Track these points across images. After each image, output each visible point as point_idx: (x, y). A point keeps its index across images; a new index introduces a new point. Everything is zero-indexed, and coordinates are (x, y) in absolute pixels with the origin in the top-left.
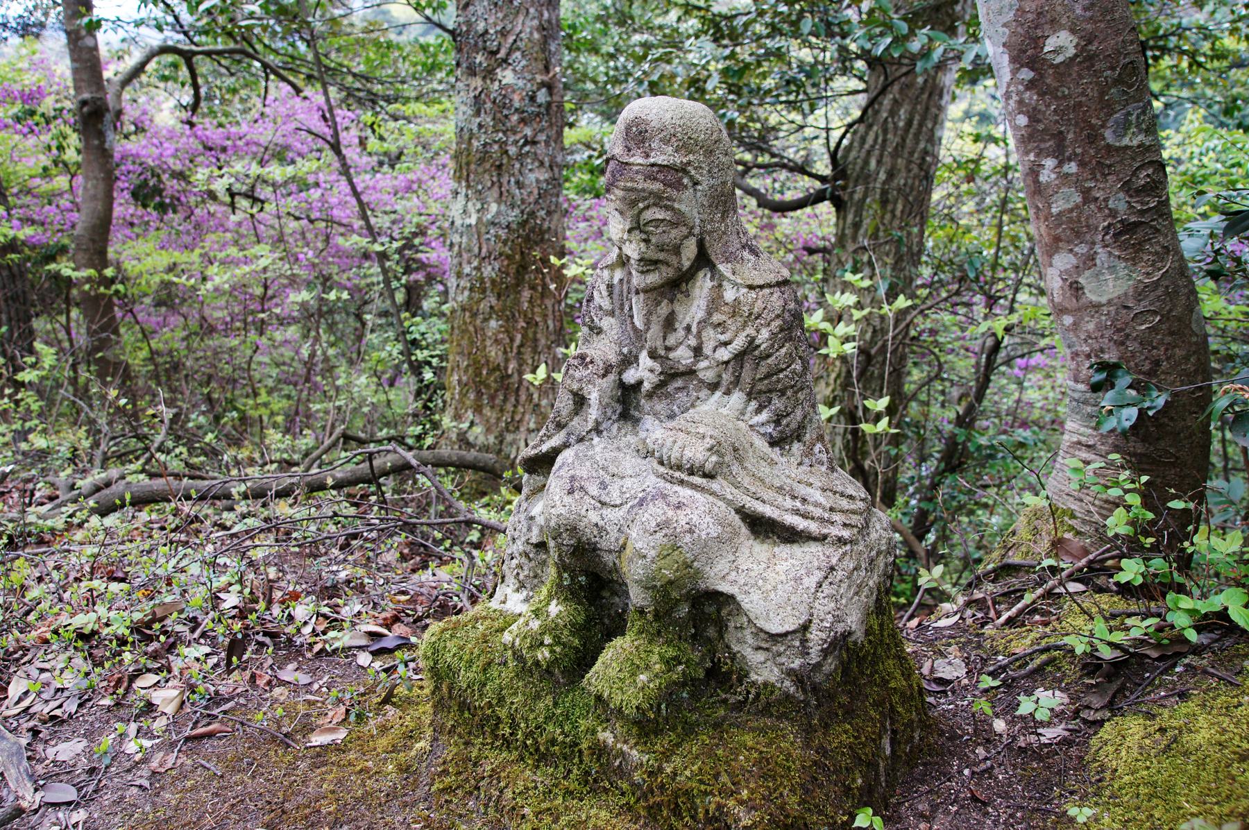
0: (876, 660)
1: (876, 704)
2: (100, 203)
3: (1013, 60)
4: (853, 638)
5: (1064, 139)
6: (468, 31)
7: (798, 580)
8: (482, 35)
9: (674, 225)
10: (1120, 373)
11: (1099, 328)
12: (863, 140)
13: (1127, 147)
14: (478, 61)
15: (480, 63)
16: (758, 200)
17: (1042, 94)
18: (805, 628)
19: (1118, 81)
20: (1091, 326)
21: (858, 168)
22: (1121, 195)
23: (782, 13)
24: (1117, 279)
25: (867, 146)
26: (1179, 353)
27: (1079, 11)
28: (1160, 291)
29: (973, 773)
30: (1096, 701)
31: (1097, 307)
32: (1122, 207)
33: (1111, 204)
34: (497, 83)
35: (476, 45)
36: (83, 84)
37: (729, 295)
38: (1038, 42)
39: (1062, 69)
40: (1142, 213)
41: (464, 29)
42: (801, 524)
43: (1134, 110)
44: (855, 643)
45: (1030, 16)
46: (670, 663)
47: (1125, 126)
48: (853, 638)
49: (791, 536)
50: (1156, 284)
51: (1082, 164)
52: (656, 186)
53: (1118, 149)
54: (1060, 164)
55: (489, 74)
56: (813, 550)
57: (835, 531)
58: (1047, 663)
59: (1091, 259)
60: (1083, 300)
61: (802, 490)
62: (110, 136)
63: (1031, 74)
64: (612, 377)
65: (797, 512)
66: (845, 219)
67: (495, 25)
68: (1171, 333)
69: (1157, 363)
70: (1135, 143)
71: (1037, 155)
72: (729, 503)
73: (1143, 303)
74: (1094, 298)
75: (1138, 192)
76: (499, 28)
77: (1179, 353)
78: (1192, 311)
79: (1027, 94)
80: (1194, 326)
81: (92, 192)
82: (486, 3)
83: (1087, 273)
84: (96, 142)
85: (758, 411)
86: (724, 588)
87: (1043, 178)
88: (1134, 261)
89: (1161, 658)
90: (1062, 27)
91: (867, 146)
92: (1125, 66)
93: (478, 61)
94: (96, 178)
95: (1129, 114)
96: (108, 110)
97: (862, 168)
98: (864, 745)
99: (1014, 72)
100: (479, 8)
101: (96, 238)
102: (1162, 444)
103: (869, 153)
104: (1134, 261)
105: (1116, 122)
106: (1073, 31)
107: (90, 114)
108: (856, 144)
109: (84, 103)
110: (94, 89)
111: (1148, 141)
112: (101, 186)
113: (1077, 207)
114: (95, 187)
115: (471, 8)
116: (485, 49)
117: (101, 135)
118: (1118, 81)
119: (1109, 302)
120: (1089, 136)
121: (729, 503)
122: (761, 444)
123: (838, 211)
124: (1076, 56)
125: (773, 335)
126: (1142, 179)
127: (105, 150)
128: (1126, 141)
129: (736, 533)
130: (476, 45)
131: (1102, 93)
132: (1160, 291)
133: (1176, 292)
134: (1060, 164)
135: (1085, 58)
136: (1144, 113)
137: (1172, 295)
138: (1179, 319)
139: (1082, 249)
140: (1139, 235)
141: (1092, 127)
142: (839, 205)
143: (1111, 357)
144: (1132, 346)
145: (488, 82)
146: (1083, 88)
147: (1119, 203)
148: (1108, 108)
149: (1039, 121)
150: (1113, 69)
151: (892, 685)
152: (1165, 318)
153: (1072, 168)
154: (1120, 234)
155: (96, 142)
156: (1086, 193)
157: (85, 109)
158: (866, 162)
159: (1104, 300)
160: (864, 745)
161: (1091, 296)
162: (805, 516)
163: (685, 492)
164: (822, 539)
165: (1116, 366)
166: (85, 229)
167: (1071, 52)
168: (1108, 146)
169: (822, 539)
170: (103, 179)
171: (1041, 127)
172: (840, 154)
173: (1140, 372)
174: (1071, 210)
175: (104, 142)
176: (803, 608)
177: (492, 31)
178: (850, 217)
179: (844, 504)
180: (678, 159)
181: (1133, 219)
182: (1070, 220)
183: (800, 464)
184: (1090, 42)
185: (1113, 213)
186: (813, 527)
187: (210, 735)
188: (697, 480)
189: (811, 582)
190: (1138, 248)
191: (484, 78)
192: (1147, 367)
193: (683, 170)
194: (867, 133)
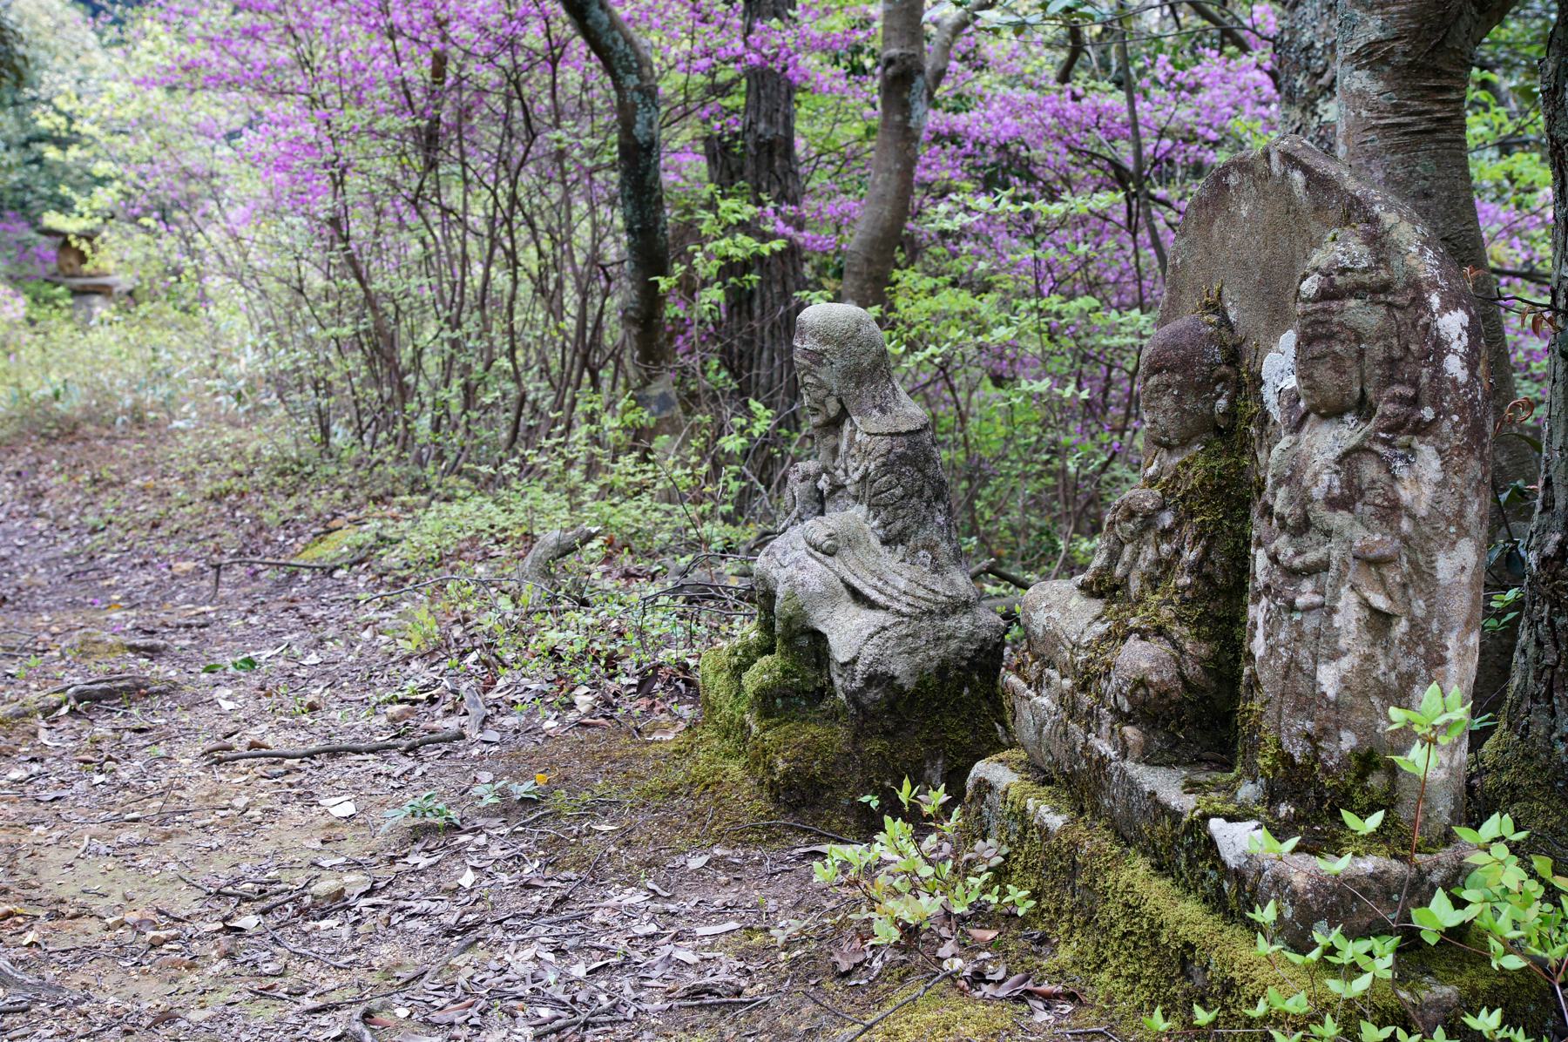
2: (888, 207)
6: (1290, 41)
7: (860, 630)
8: (1307, 49)
9: (820, 387)
14: (1298, 84)
15: (1302, 88)
18: (854, 661)
34: (1316, 118)
35: (1297, 62)
36: (893, 34)
37: (858, 437)
41: (1287, 38)
42: (874, 595)
46: (785, 672)
49: (873, 605)
52: (807, 362)
55: (1309, 106)
56: (879, 617)
57: (896, 606)
61: (890, 577)
62: (919, 107)
64: (809, 483)
65: (875, 588)
67: (1326, 35)
72: (837, 574)
76: (1328, 41)
81: (880, 190)
82: (1317, 5)
84: (898, 118)
85: (875, 517)
86: (822, 628)
93: (1298, 84)
94: (889, 171)
96: (921, 71)
100: (1309, 10)
101: (875, 258)
107: (895, 78)
109: (890, 61)
110: (906, 41)
112: (895, 181)
114: (886, 183)
115: (1300, 8)
116: (1308, 69)
117: (906, 108)
121: (837, 574)
122: (875, 542)
125: (877, 468)
127: (909, 129)
129: (837, 594)
130: (1297, 62)
145: (1308, 115)
155: (898, 118)
157: (890, 71)
162: (881, 592)
163: (811, 561)
164: (887, 608)
166: (861, 243)
169: (887, 608)
170: (899, 172)
175: (910, 117)
176: (855, 648)
177: (1319, 45)
179: (931, 596)
180: (818, 347)
183: (903, 561)
186: (882, 599)
187: (594, 725)
188: (818, 554)
189: (866, 633)
191: (1304, 109)
193: (822, 353)
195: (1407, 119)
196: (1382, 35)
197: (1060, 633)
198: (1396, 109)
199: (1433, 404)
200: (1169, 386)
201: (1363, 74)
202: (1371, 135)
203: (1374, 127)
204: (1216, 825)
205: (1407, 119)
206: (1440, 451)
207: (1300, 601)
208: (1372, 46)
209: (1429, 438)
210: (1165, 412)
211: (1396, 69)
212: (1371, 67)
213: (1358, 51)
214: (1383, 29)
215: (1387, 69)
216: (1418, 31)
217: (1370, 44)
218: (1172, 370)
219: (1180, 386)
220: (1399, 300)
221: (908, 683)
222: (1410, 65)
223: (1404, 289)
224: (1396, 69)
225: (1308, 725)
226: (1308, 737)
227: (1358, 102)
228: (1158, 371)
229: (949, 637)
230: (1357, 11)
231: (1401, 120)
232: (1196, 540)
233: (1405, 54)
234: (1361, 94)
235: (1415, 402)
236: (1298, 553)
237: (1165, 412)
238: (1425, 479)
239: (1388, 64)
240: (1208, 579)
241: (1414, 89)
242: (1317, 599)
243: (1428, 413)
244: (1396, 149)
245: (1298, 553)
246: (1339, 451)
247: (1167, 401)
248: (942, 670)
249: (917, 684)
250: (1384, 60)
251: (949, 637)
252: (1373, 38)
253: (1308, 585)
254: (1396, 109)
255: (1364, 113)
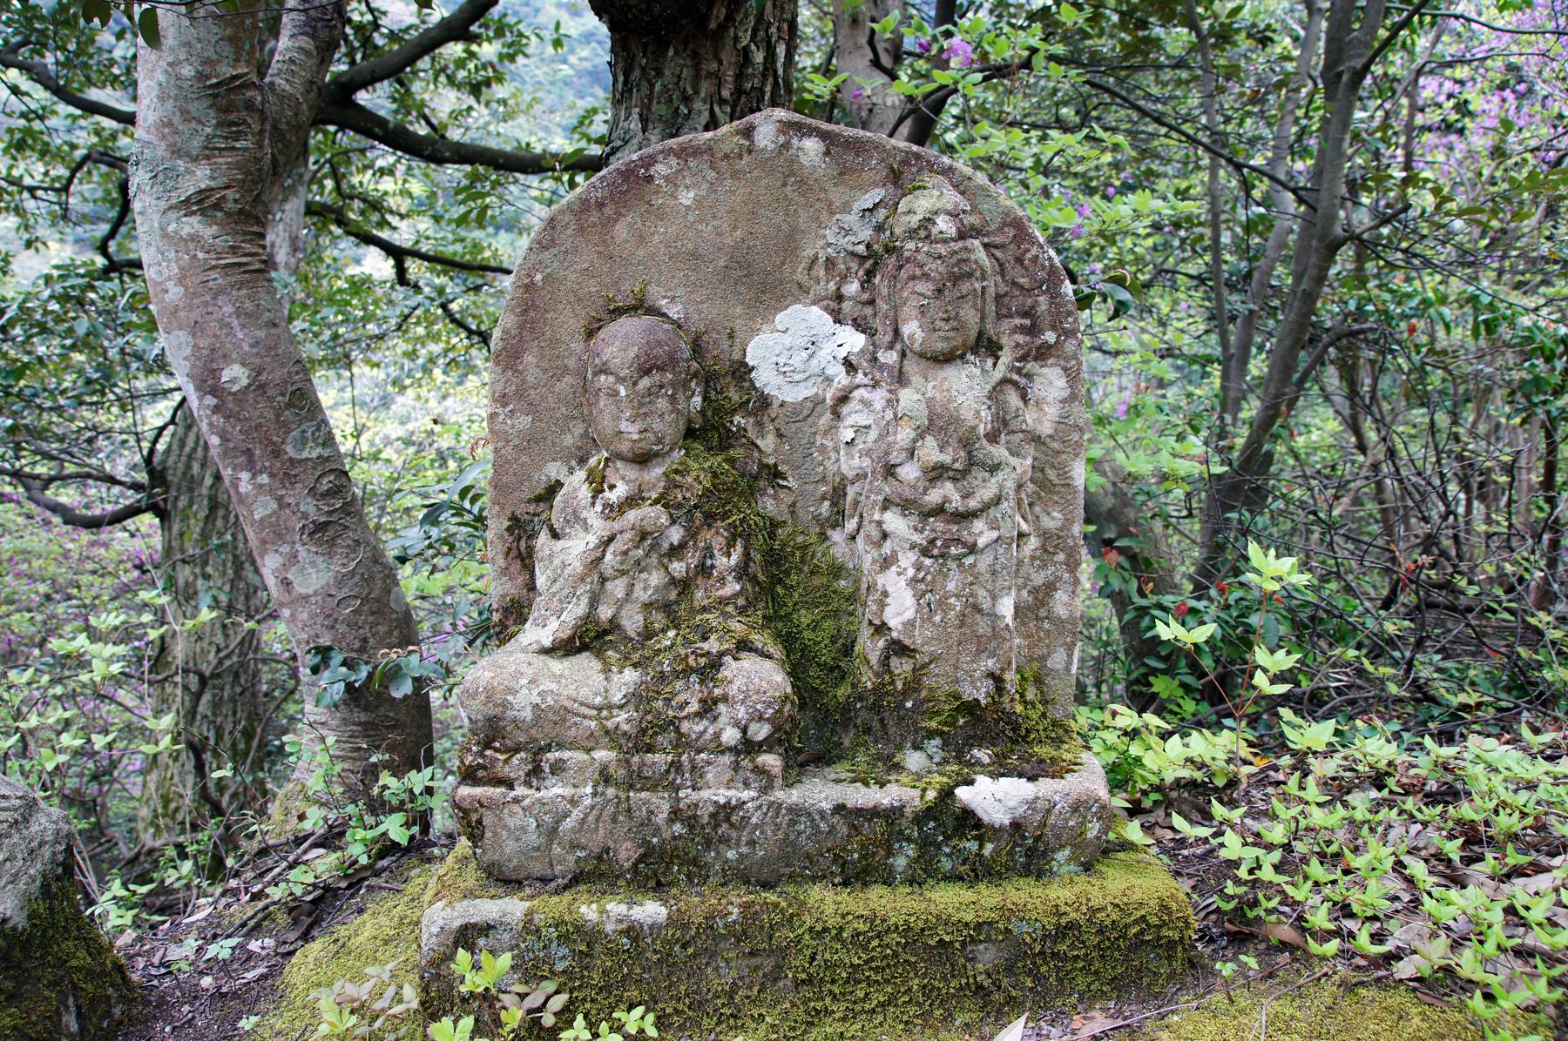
0: (46, 943)
1: (52, 985)
3: (198, 388)
4: (11, 924)
5: (253, 455)
10: (333, 654)
11: (312, 616)
12: (182, 443)
13: (307, 459)
16: (63, 516)
17: (227, 417)
19: (289, 405)
20: (305, 616)
21: (179, 473)
22: (309, 499)
23: (53, 312)
24: (318, 572)
25: (187, 450)
26: (382, 629)
27: (246, 348)
28: (357, 578)
29: (174, 1028)
30: (292, 936)
31: (306, 598)
32: (311, 510)
33: (302, 508)
38: (215, 373)
39: (240, 396)
40: (330, 513)
43: (310, 428)
44: (14, 928)
45: (205, 352)
47: (303, 441)
48: (11, 924)
50: (353, 573)
51: (272, 475)
53: (300, 461)
54: (254, 476)
58: (264, 919)
59: (293, 557)
60: (294, 594)
63: (214, 401)
66: (170, 529)
68: (373, 613)
69: (365, 640)
70: (314, 455)
71: (234, 469)
73: (345, 590)
74: (303, 591)
75: (324, 496)
77: (382, 629)
78: (389, 592)
79: (215, 418)
80: (392, 605)
83: (293, 569)
87: (242, 490)
88: (330, 555)
89: (349, 887)
90: (233, 361)
91: (187, 450)
92: (293, 393)
95: (304, 431)
97: (184, 474)
98: (35, 1024)
99: (201, 399)
102: (382, 711)
103: (190, 457)
104: (330, 555)
105: (295, 439)
106: (243, 364)
108: (175, 447)
111: (326, 453)
113: (274, 512)
118: (289, 405)
119: (316, 593)
120: (273, 452)
123: (162, 521)
124: (250, 385)
126: (325, 485)
128: (305, 454)
131: (278, 416)
132: (357, 578)
133: (372, 578)
134: (254, 476)
135: (258, 386)
136: (318, 429)
137: (368, 580)
138: (378, 600)
139: (285, 549)
140: (330, 532)
141: (274, 444)
142: (162, 514)
143: (325, 641)
144: (342, 628)
146: (260, 411)
147: (309, 506)
148: (286, 427)
149: (228, 440)
150: (283, 395)
151: (74, 963)
152: (365, 600)
153: (264, 479)
154: (314, 532)
156: (280, 499)
158: (188, 467)
159: (310, 591)
160: (35, 1024)
161: (300, 589)
165: (330, 649)
167: (245, 382)
168: (291, 459)
171: (231, 445)
172: (156, 459)
173: (353, 650)
174: (270, 516)
178: (176, 528)
181: (323, 519)
182: (271, 525)
184: (259, 373)
185: (305, 516)
190: (332, 543)
192: (357, 645)
194: (186, 435)
195: (244, 260)
196: (213, 184)
197: (569, 704)
198: (234, 250)
199: (1053, 328)
200: (661, 387)
201: (195, 220)
202: (213, 275)
203: (214, 267)
204: (962, 793)
205: (244, 260)
206: (1065, 369)
207: (981, 542)
208: (204, 195)
209: (1051, 361)
210: (661, 416)
211: (228, 214)
212: (203, 212)
213: (188, 200)
214: (212, 178)
215: (219, 214)
216: (244, 181)
217: (200, 192)
218: (661, 369)
219: (673, 385)
220: (997, 240)
221: (19, 920)
222: (241, 211)
223: (1001, 229)
224: (228, 214)
225: (990, 663)
226: (991, 675)
227: (191, 246)
228: (647, 372)
229: (41, 845)
230: (180, 162)
231: (236, 260)
232: (730, 544)
233: (236, 201)
234: (194, 238)
235: (1033, 331)
236: (966, 496)
237: (661, 416)
238: (1050, 399)
239: (221, 210)
240: (754, 579)
241: (245, 233)
242: (995, 534)
243: (1050, 337)
244: (241, 285)
245: (966, 496)
246: (989, 387)
247: (662, 404)
248: (45, 888)
249: (30, 917)
250: (217, 206)
251: (41, 845)
252: (203, 186)
253: (978, 525)
254: (234, 250)
255: (201, 255)
